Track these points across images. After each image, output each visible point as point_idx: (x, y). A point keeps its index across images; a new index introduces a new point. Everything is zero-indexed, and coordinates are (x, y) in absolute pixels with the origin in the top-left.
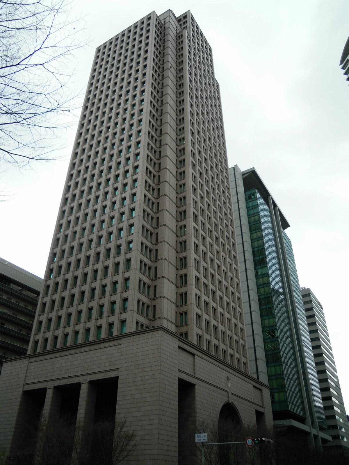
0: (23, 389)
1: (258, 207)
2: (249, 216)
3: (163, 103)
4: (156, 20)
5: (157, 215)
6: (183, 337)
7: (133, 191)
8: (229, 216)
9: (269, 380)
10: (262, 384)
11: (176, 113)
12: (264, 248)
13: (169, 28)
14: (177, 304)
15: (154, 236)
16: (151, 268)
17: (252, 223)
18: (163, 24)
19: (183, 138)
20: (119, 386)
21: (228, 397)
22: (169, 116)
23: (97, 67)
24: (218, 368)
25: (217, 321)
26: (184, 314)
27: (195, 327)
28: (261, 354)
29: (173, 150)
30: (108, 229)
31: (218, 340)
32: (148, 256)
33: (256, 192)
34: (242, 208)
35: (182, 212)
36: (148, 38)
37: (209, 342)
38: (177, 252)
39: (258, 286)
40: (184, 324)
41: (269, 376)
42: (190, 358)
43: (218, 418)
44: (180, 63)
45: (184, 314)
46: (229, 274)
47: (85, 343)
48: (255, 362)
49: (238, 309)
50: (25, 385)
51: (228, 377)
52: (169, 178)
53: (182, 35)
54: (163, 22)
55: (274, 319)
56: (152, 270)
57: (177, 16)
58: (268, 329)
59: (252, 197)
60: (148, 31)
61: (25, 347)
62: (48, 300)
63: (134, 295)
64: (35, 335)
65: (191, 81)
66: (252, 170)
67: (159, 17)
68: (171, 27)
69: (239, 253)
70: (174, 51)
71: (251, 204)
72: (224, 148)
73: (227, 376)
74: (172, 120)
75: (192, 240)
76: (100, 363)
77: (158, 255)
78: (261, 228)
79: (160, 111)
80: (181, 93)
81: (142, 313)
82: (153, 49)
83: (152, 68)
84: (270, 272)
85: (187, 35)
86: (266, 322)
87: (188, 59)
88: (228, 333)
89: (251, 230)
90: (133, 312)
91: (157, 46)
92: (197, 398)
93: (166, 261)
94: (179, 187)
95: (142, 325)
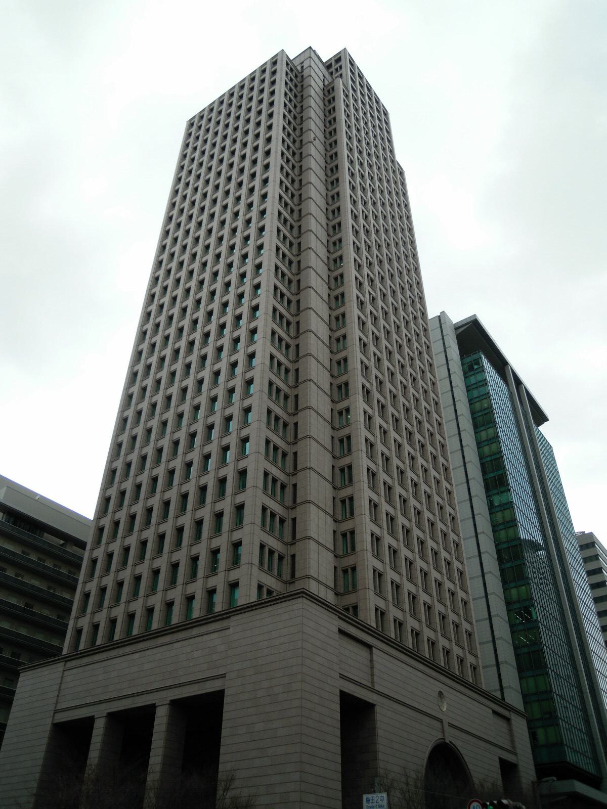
0: (53, 720)
1: (486, 384)
2: (471, 402)
3: (302, 268)
4: (287, 64)
5: (295, 392)
6: (350, 613)
7: (246, 403)
8: (432, 395)
9: (525, 703)
10: (510, 708)
11: (327, 215)
12: (502, 457)
13: (310, 76)
14: (337, 552)
15: (291, 428)
16: (286, 487)
17: (478, 412)
18: (300, 71)
19: (344, 359)
20: (226, 708)
21: (443, 732)
22: (313, 236)
23: (181, 186)
24: (419, 674)
25: (416, 585)
26: (350, 570)
27: (372, 593)
28: (507, 653)
29: (321, 278)
30: (203, 449)
31: (419, 621)
32: (279, 498)
33: (481, 358)
34: (457, 386)
35: (342, 411)
36: (270, 127)
37: (400, 625)
38: (334, 457)
39: (493, 527)
40: (350, 589)
41: (525, 696)
42: (363, 653)
43: (425, 765)
44: (335, 244)
45: (350, 570)
46: (440, 526)
47: (164, 629)
48: (491, 644)
49: (461, 594)
50: (56, 712)
51: (440, 693)
52: (317, 323)
53: (333, 88)
54: (299, 68)
55: (512, 509)
56: (289, 428)
57: (324, 61)
58: (518, 606)
59: (476, 367)
60: (271, 116)
61: (56, 642)
62: (100, 553)
63: (252, 534)
64: (77, 618)
65: (356, 217)
66: (472, 319)
67: (294, 62)
68: (313, 74)
69: (456, 486)
70: (321, 125)
71: (473, 380)
72: (424, 324)
73: (439, 690)
74: (318, 195)
75: (361, 434)
76: (191, 665)
77: (299, 404)
78: (495, 421)
79: (295, 325)
80: (335, 182)
81: (270, 568)
82: (282, 122)
83: (279, 183)
84: (515, 500)
85: (342, 87)
86: (514, 592)
87: (348, 162)
88: (438, 607)
89: (476, 426)
90: (256, 489)
91: (289, 105)
92: (380, 732)
93: (312, 542)
94: (335, 342)
95: (270, 592)
